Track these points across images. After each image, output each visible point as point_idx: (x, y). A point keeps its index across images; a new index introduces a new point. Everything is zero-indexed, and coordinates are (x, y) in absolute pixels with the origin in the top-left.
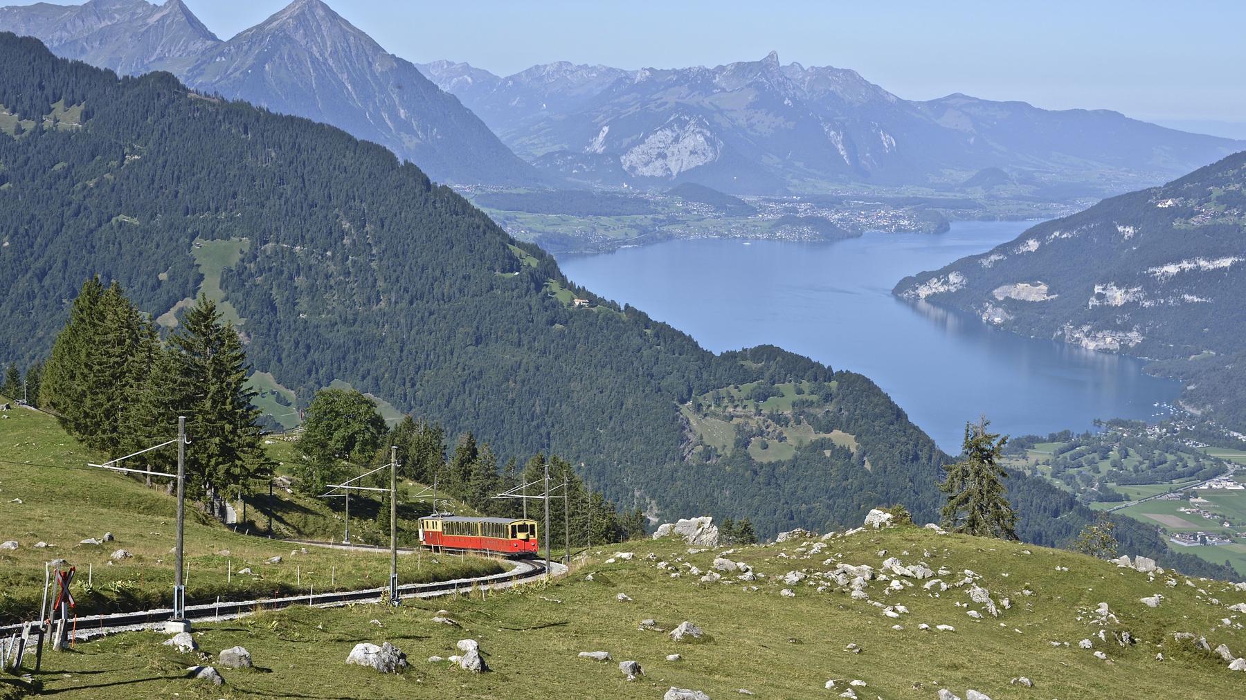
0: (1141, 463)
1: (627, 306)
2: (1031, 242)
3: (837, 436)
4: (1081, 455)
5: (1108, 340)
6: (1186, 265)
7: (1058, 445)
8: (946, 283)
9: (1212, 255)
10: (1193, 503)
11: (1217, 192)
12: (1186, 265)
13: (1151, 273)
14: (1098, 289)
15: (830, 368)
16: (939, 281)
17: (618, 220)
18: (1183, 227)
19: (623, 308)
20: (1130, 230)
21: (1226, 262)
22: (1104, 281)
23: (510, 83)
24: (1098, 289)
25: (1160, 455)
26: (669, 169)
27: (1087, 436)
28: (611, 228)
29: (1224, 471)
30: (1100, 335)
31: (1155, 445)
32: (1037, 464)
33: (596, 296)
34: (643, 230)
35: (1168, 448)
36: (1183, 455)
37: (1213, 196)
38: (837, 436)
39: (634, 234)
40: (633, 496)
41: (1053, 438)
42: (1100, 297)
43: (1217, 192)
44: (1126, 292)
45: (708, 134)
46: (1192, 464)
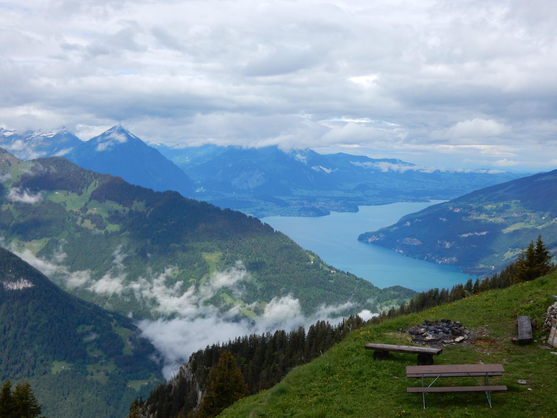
1: (348, 272)
2: (408, 223)
5: (446, 260)
6: (470, 234)
9: (479, 231)
12: (470, 234)
13: (459, 237)
16: (376, 236)
17: (244, 210)
19: (346, 273)
21: (484, 233)
23: (408, 224)
26: (249, 187)
30: (443, 259)
44: (450, 244)
45: (263, 173)
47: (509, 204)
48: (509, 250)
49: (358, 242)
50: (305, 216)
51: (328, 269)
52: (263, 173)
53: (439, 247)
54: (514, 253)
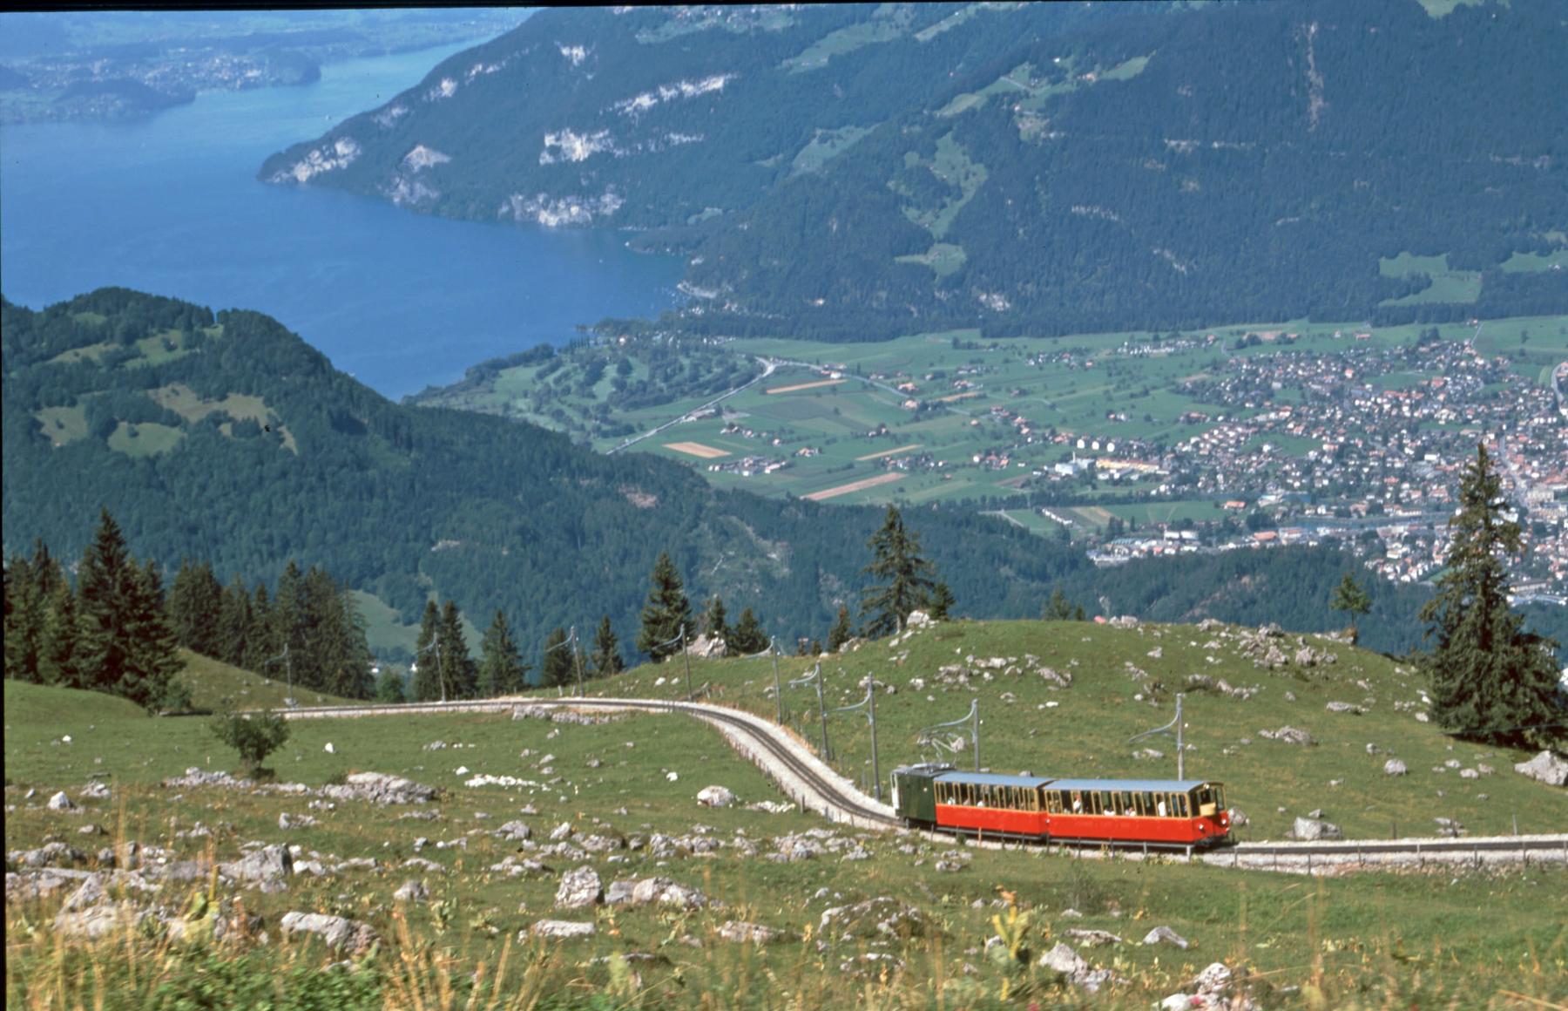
14: (549, 140)
15: (207, 309)
22: (556, 128)
42: (555, 150)
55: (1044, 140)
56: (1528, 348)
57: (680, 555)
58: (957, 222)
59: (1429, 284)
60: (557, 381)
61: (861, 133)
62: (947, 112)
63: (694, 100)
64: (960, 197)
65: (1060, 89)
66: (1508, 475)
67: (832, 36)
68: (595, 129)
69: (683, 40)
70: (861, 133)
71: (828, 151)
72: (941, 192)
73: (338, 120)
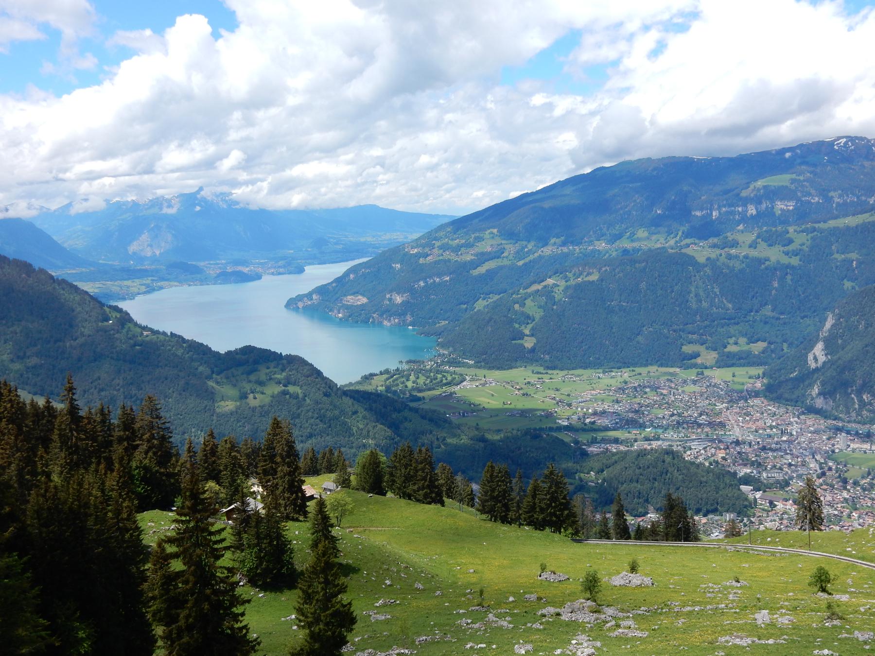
0: (426, 380)
1: (171, 333)
3: (291, 389)
4: (397, 379)
7: (385, 376)
8: (312, 299)
10: (455, 397)
11: (437, 244)
14: (388, 296)
15: (281, 353)
17: (133, 282)
18: (424, 262)
19: (169, 334)
20: (398, 266)
22: (391, 291)
24: (388, 296)
25: (434, 375)
27: (398, 370)
28: (134, 285)
29: (464, 380)
31: (431, 371)
32: (377, 387)
33: (336, 385)
34: (148, 286)
35: (438, 372)
36: (445, 374)
37: (436, 246)
38: (291, 389)
39: (143, 289)
40: (191, 431)
41: (381, 373)
42: (390, 300)
43: (437, 244)
44: (402, 296)
45: (173, 232)
46: (449, 378)
47: (482, 235)
48: (481, 297)
49: (285, 310)
50: (224, 284)
51: (139, 330)
52: (173, 232)
53: (388, 303)
54: (487, 301)
55: (564, 302)
56: (736, 379)
57: (251, 449)
58: (532, 329)
59: (699, 356)
60: (393, 381)
61: (497, 297)
62: (529, 290)
63: (439, 284)
64: (534, 320)
65: (568, 283)
66: (115, 414)
67: (487, 263)
68: (405, 292)
69: (436, 262)
70: (497, 297)
71: (485, 303)
72: (528, 318)
73: (314, 287)
